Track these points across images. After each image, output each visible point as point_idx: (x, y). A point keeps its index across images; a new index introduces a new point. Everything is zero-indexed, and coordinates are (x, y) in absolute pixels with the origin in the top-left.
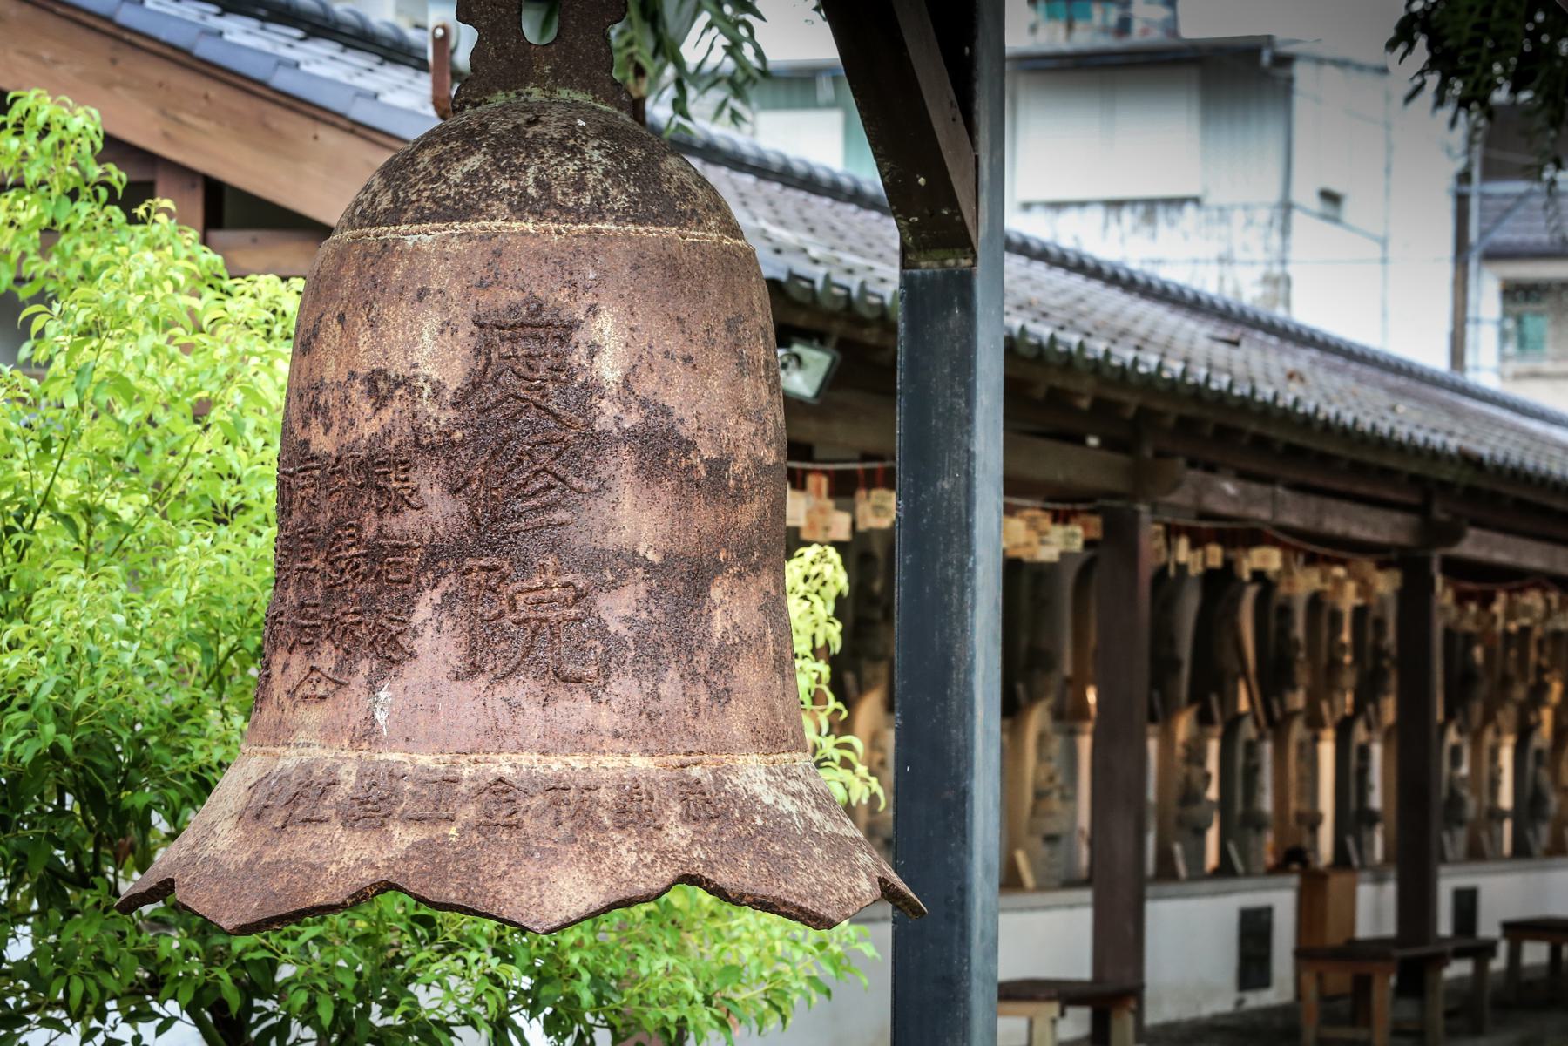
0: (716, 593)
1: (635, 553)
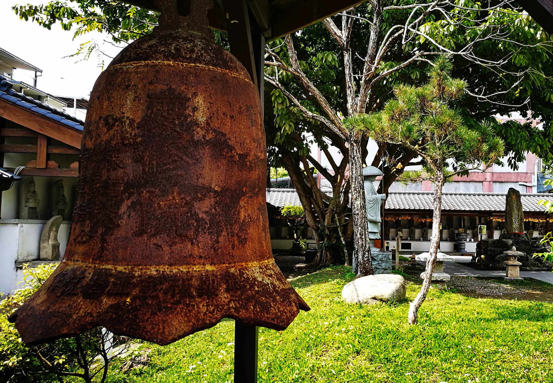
0: (242, 203)
1: (211, 187)
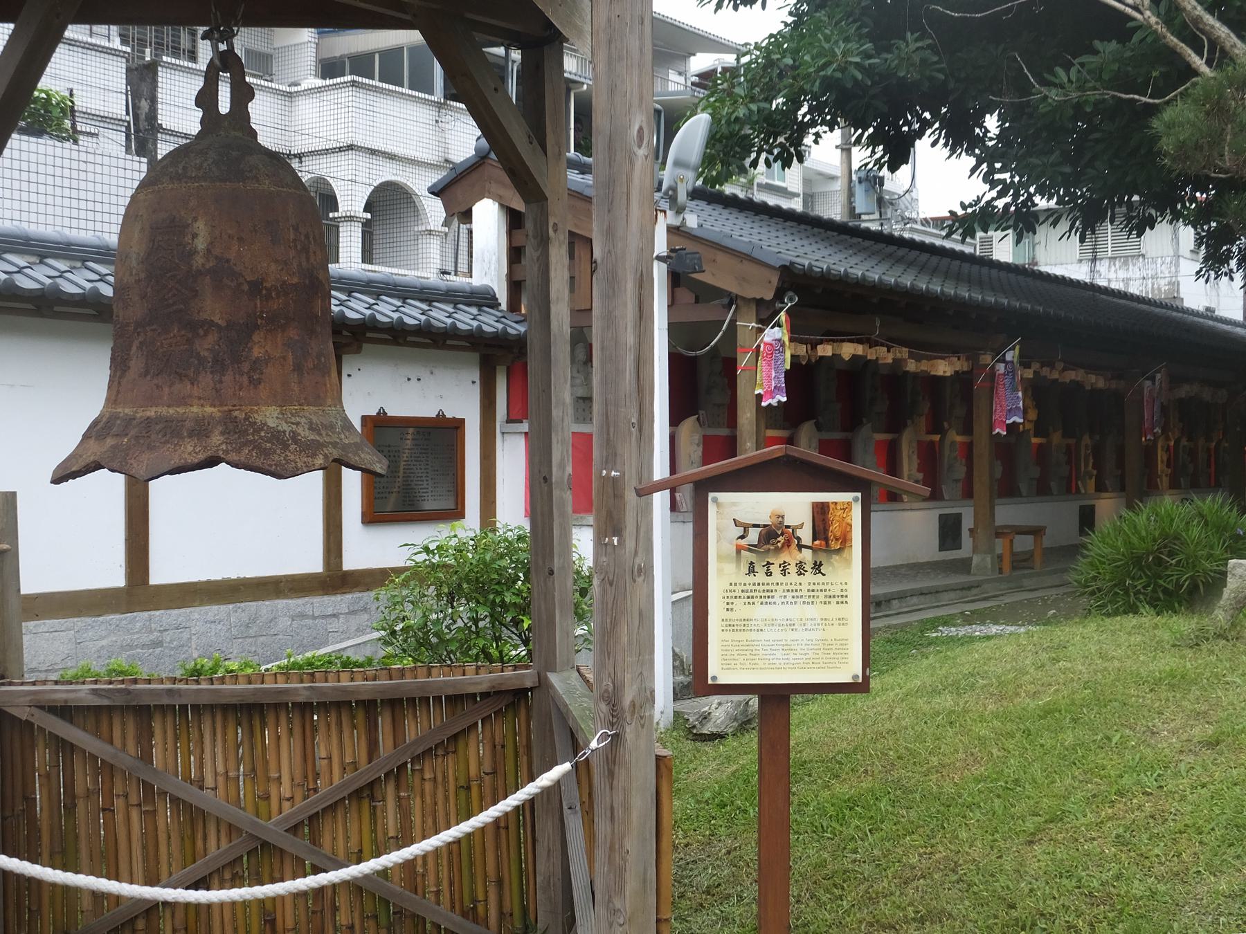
0: (256, 338)
